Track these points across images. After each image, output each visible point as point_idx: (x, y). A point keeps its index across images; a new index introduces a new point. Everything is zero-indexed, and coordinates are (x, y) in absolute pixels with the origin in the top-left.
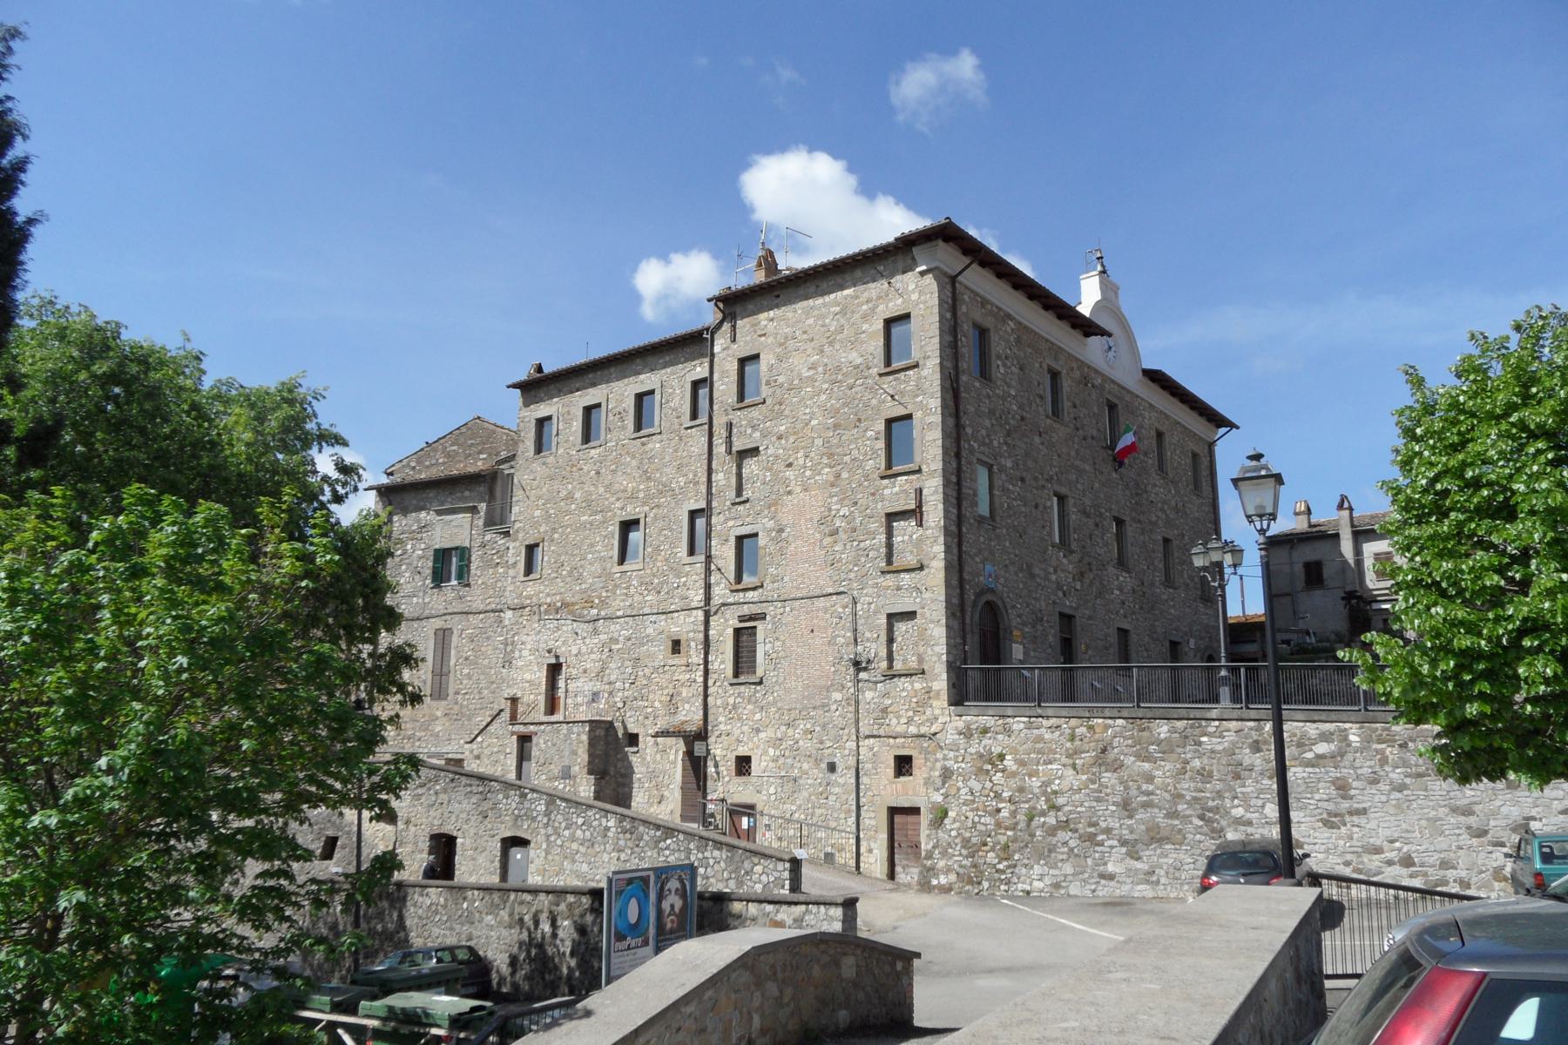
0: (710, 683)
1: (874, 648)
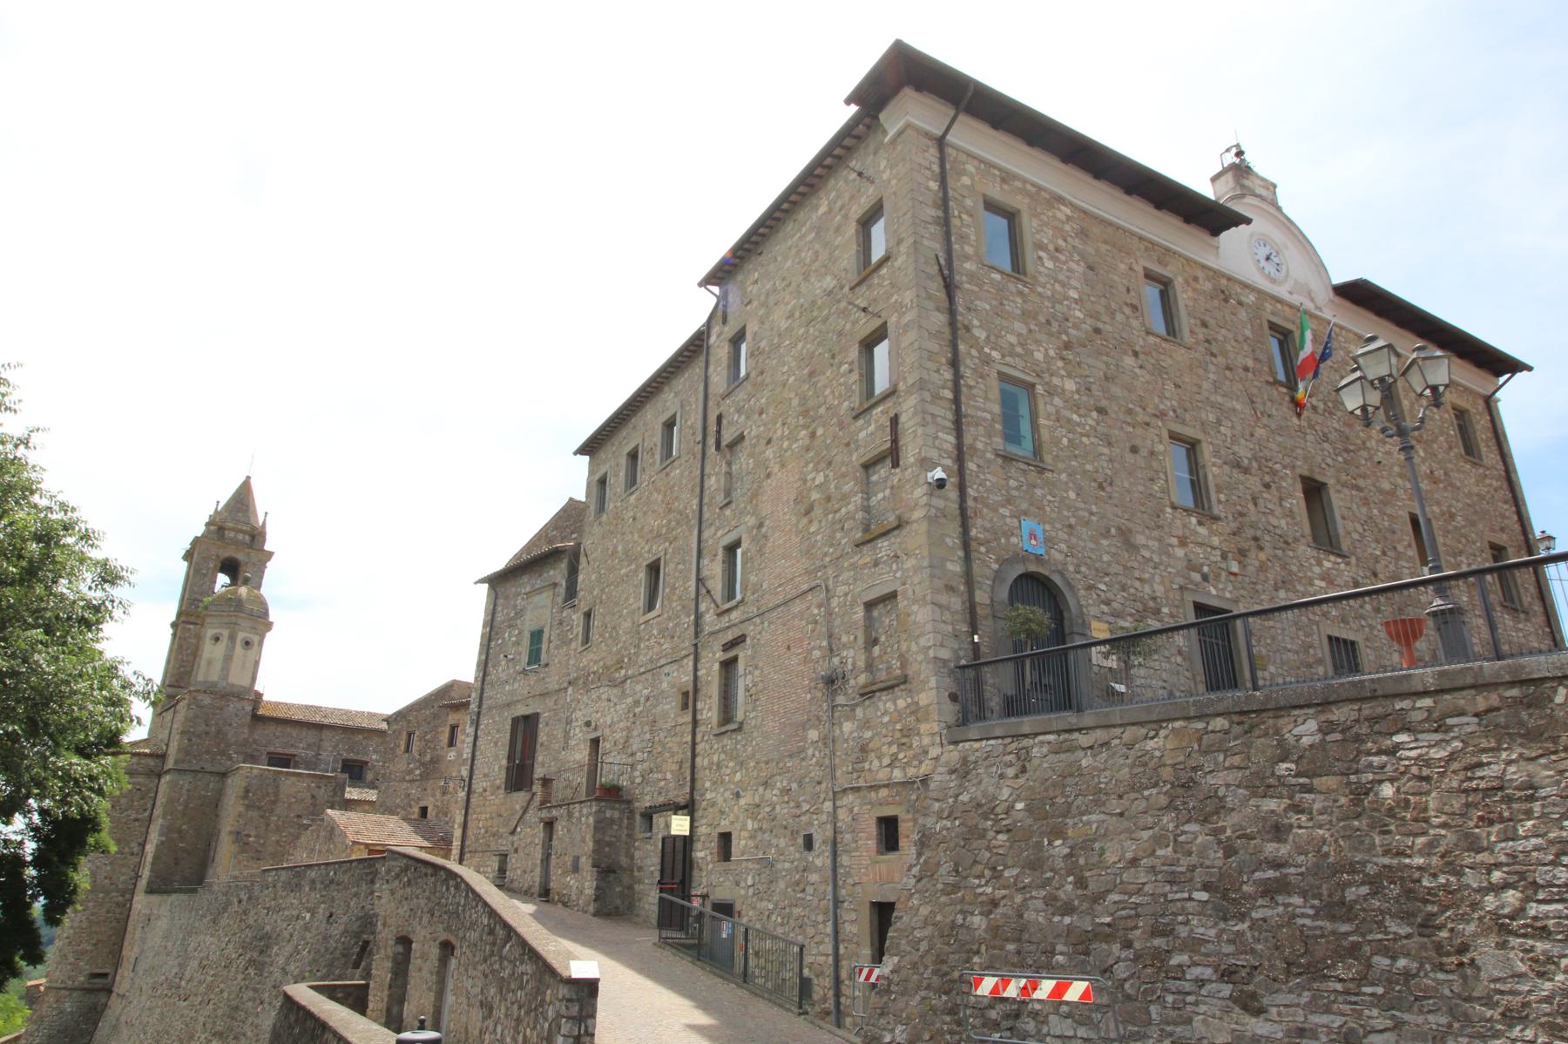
0: (698, 738)
1: (853, 657)
